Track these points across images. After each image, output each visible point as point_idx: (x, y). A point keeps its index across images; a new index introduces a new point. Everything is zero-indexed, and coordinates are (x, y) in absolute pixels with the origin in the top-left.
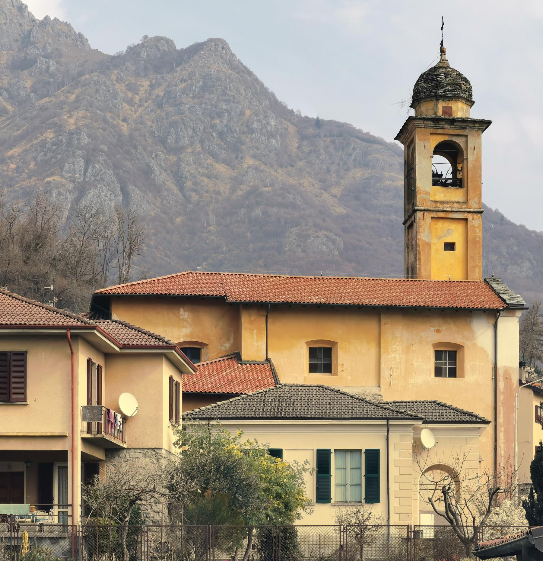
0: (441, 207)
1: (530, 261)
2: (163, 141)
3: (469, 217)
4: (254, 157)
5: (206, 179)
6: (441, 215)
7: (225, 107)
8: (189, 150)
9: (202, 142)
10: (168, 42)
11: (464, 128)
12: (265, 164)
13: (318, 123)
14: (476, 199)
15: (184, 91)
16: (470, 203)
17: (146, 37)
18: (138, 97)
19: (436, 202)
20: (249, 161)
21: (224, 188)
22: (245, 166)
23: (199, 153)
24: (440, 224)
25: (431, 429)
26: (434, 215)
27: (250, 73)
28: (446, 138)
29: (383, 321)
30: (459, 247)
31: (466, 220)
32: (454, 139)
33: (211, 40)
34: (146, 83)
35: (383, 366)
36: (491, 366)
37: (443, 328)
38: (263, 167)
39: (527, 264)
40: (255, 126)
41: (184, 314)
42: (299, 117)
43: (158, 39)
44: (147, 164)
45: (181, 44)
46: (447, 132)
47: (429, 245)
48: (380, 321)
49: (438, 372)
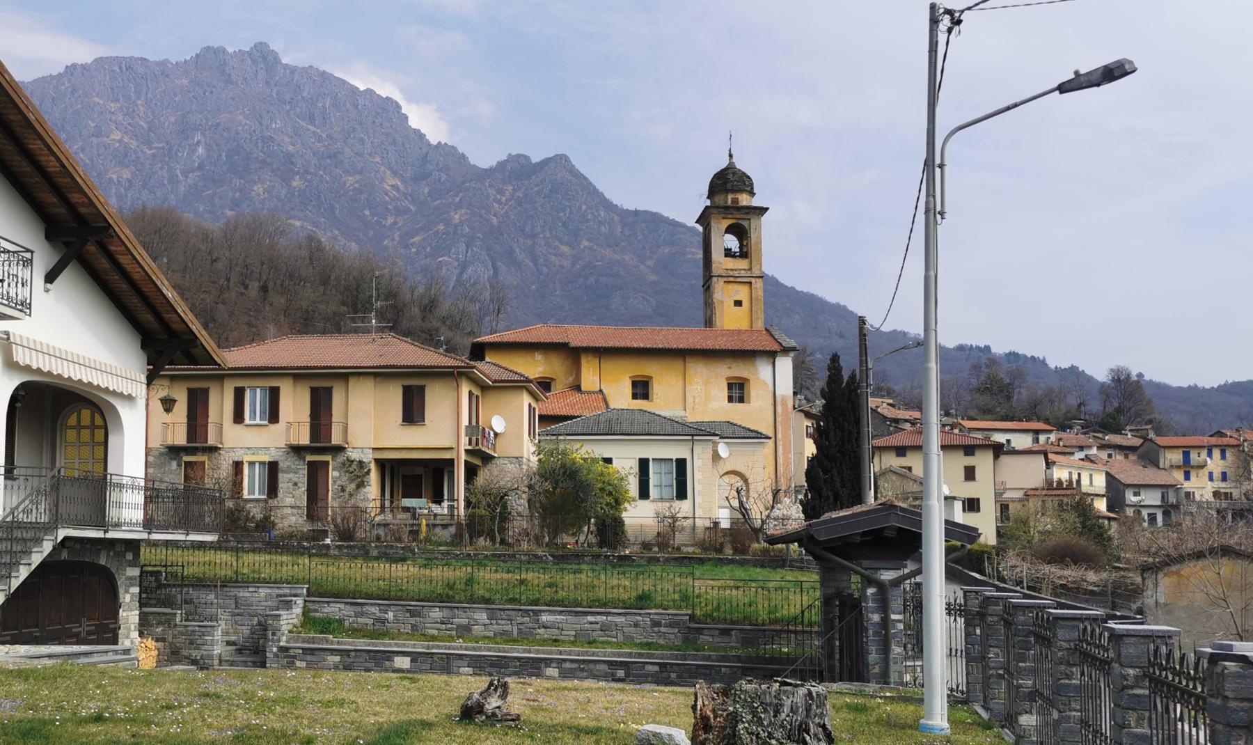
0: (731, 273)
1: (800, 315)
2: (522, 230)
3: (753, 280)
4: (588, 240)
5: (553, 258)
6: (732, 279)
7: (567, 204)
8: (541, 236)
9: (550, 230)
10: (526, 157)
11: (748, 213)
12: (597, 245)
13: (636, 212)
14: (758, 267)
15: (538, 193)
16: (753, 269)
17: (510, 154)
18: (504, 198)
19: (727, 270)
20: (585, 243)
21: (567, 263)
22: (582, 247)
23: (549, 238)
24: (730, 286)
25: (725, 443)
26: (726, 279)
27: (585, 179)
28: (734, 221)
29: (687, 360)
30: (745, 304)
31: (750, 283)
32: (740, 222)
33: (557, 155)
34: (510, 188)
35: (687, 394)
36: (771, 395)
37: (734, 365)
38: (595, 247)
39: (797, 316)
40: (589, 217)
41: (539, 357)
42: (622, 209)
43: (519, 156)
44: (511, 247)
45: (535, 159)
46: (735, 216)
47: (722, 302)
48: (685, 361)
49: (730, 400)
